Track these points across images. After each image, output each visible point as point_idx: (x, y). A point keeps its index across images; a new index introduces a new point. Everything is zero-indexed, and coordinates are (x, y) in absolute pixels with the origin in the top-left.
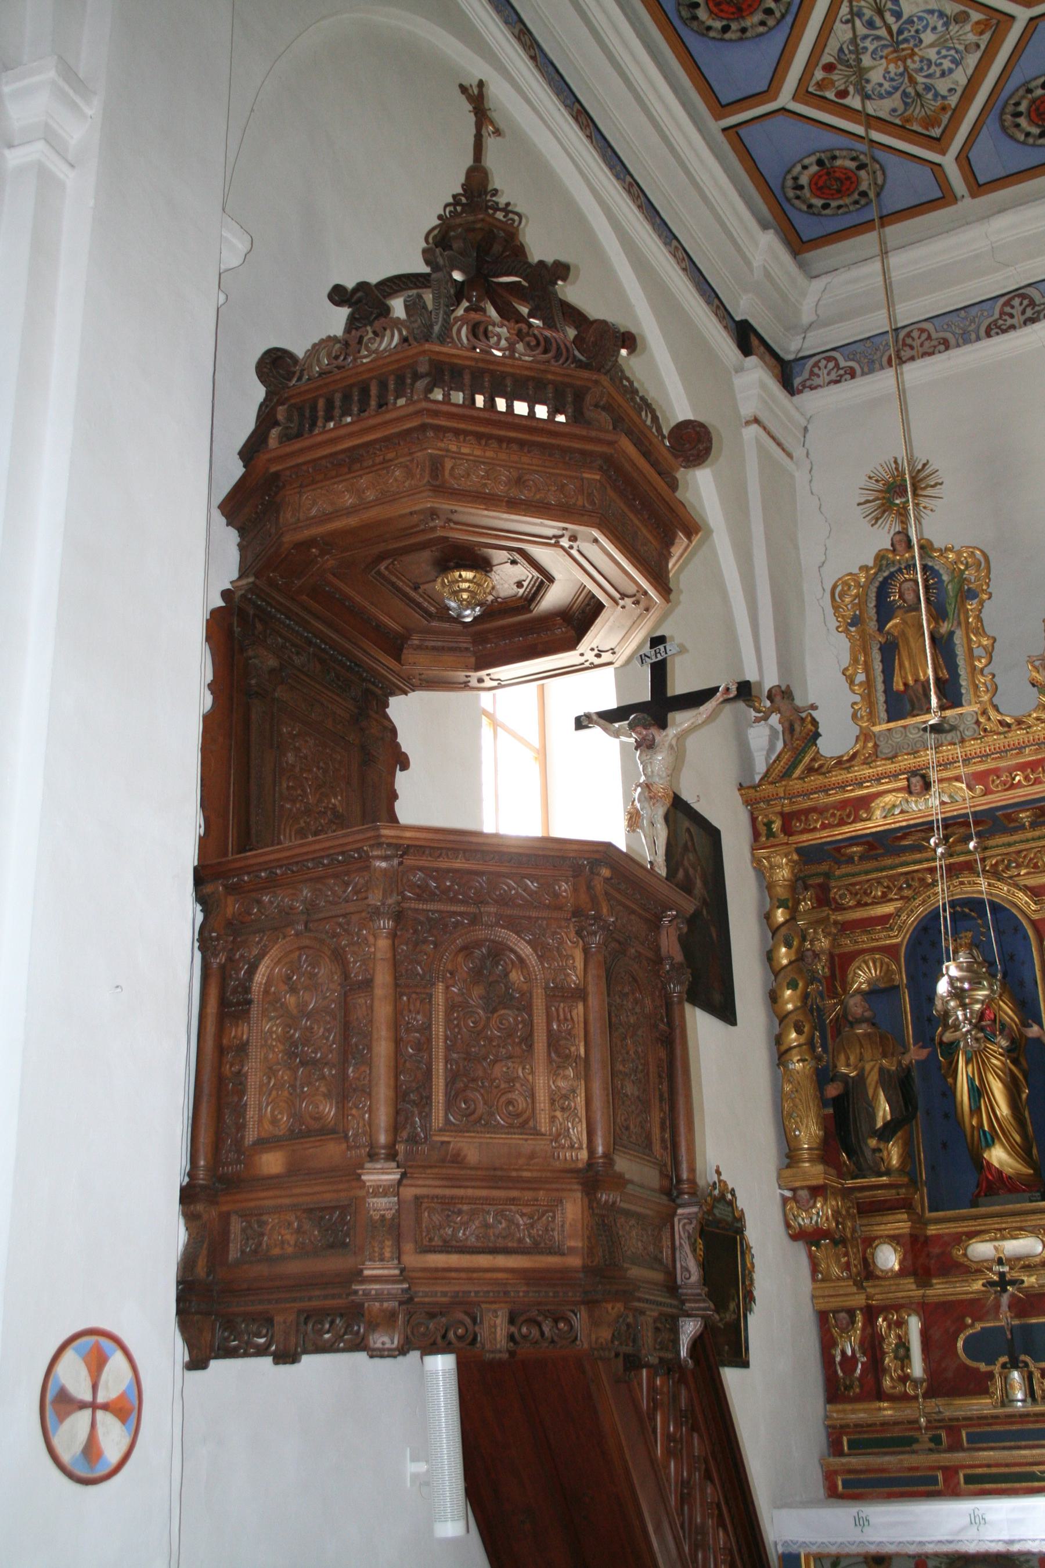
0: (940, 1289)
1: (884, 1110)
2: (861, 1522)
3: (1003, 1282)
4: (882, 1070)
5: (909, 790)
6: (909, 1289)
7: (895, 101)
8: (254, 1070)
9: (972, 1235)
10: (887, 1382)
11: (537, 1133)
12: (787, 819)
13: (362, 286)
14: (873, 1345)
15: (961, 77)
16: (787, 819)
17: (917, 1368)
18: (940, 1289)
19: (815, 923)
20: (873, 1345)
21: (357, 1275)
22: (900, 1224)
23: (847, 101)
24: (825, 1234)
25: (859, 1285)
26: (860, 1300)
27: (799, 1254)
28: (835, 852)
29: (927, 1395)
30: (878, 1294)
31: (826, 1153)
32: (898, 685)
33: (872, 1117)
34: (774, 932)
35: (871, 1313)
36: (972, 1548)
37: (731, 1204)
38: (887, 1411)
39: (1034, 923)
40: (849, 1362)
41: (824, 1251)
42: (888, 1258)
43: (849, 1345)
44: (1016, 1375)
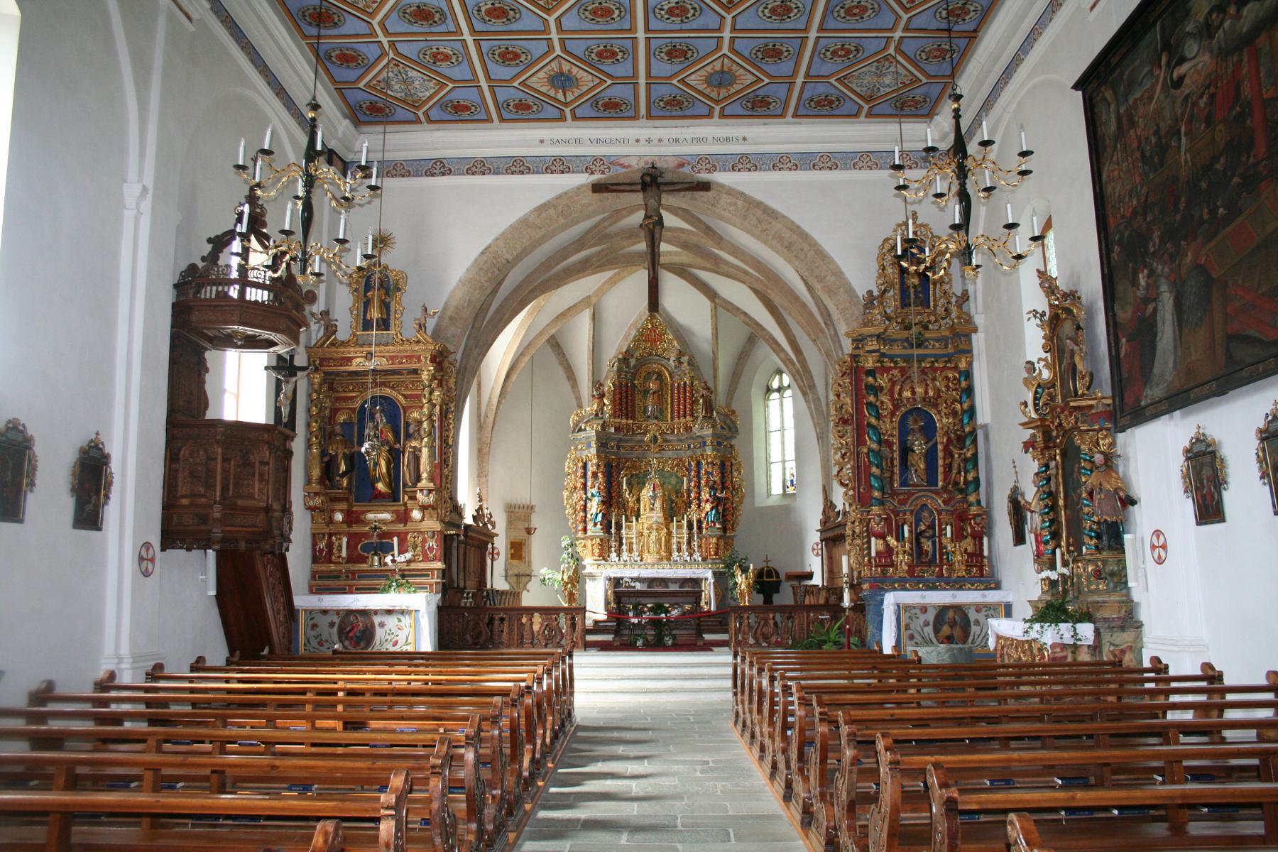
0: (355, 528)
1: (343, 468)
2: (320, 600)
3: (376, 528)
4: (344, 454)
5: (366, 357)
6: (345, 528)
8: (180, 476)
10: (333, 558)
11: (255, 499)
12: (322, 360)
13: (217, 237)
14: (330, 546)
16: (322, 360)
17: (344, 554)
18: (355, 528)
19: (326, 397)
20: (330, 546)
21: (210, 531)
22: (344, 506)
24: (318, 508)
26: (327, 531)
27: (308, 514)
28: (338, 374)
29: (347, 562)
30: (333, 529)
31: (321, 481)
33: (339, 469)
34: (312, 401)
35: (330, 535)
36: (354, 608)
38: (332, 567)
39: (403, 407)
40: (321, 551)
41: (317, 512)
42: (339, 517)
43: (322, 545)
44: (376, 558)
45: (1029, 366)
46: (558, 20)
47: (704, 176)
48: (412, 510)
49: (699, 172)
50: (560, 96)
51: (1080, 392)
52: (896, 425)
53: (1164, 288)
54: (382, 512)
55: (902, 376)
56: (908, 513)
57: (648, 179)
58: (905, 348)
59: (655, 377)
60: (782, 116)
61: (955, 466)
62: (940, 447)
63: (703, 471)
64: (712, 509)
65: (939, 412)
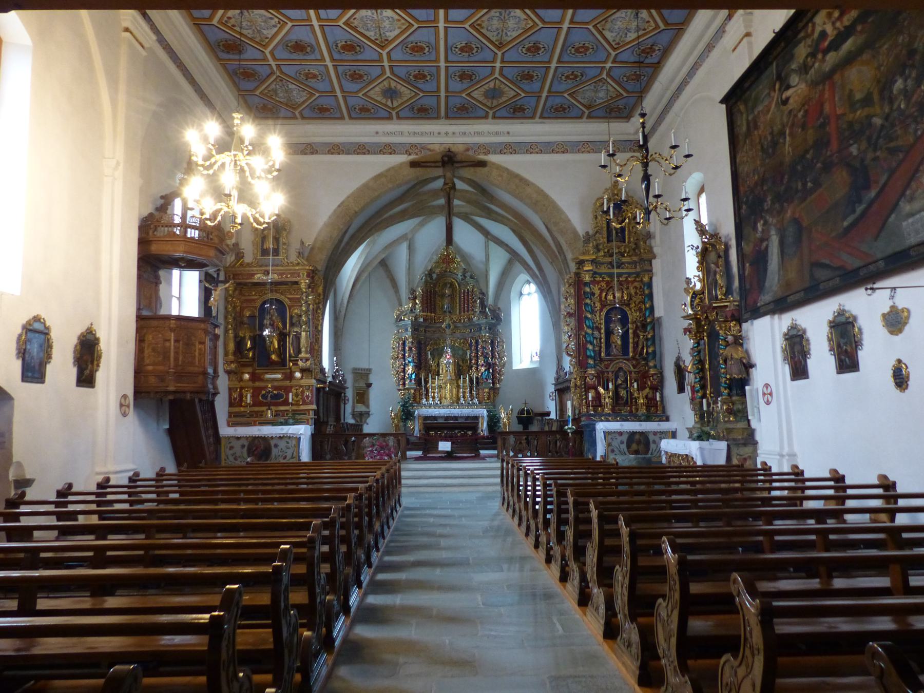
0: (257, 384)
2: (236, 430)
6: (250, 384)
7: (285, 100)
9: (267, 373)
14: (241, 396)
15: (302, 100)
16: (234, 275)
18: (257, 384)
22: (250, 370)
23: (235, 28)
25: (239, 382)
32: (265, 247)
35: (241, 388)
37: (95, 335)
38: (242, 409)
40: (235, 399)
42: (247, 376)
43: (235, 395)
45: (687, 280)
46: (389, 54)
47: (482, 157)
48: (295, 372)
49: (479, 155)
50: (389, 103)
51: (720, 297)
52: (603, 317)
53: (773, 232)
54: (275, 373)
55: (607, 286)
56: (610, 373)
57: (446, 159)
58: (609, 268)
59: (449, 286)
60: (532, 117)
61: (640, 343)
62: (631, 331)
63: (480, 346)
64: (485, 370)
65: (631, 309)
